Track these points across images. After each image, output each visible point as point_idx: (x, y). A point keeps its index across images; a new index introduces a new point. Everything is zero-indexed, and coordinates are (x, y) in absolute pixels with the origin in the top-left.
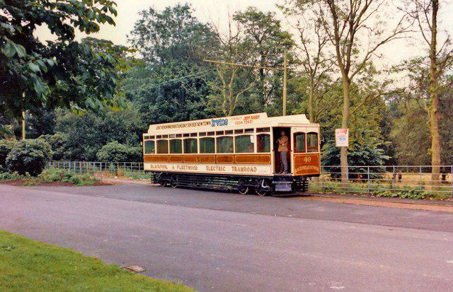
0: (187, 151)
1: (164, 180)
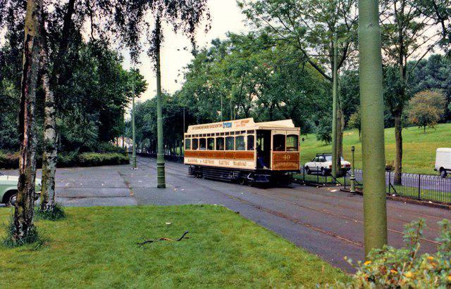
0: (227, 149)
1: (197, 172)
